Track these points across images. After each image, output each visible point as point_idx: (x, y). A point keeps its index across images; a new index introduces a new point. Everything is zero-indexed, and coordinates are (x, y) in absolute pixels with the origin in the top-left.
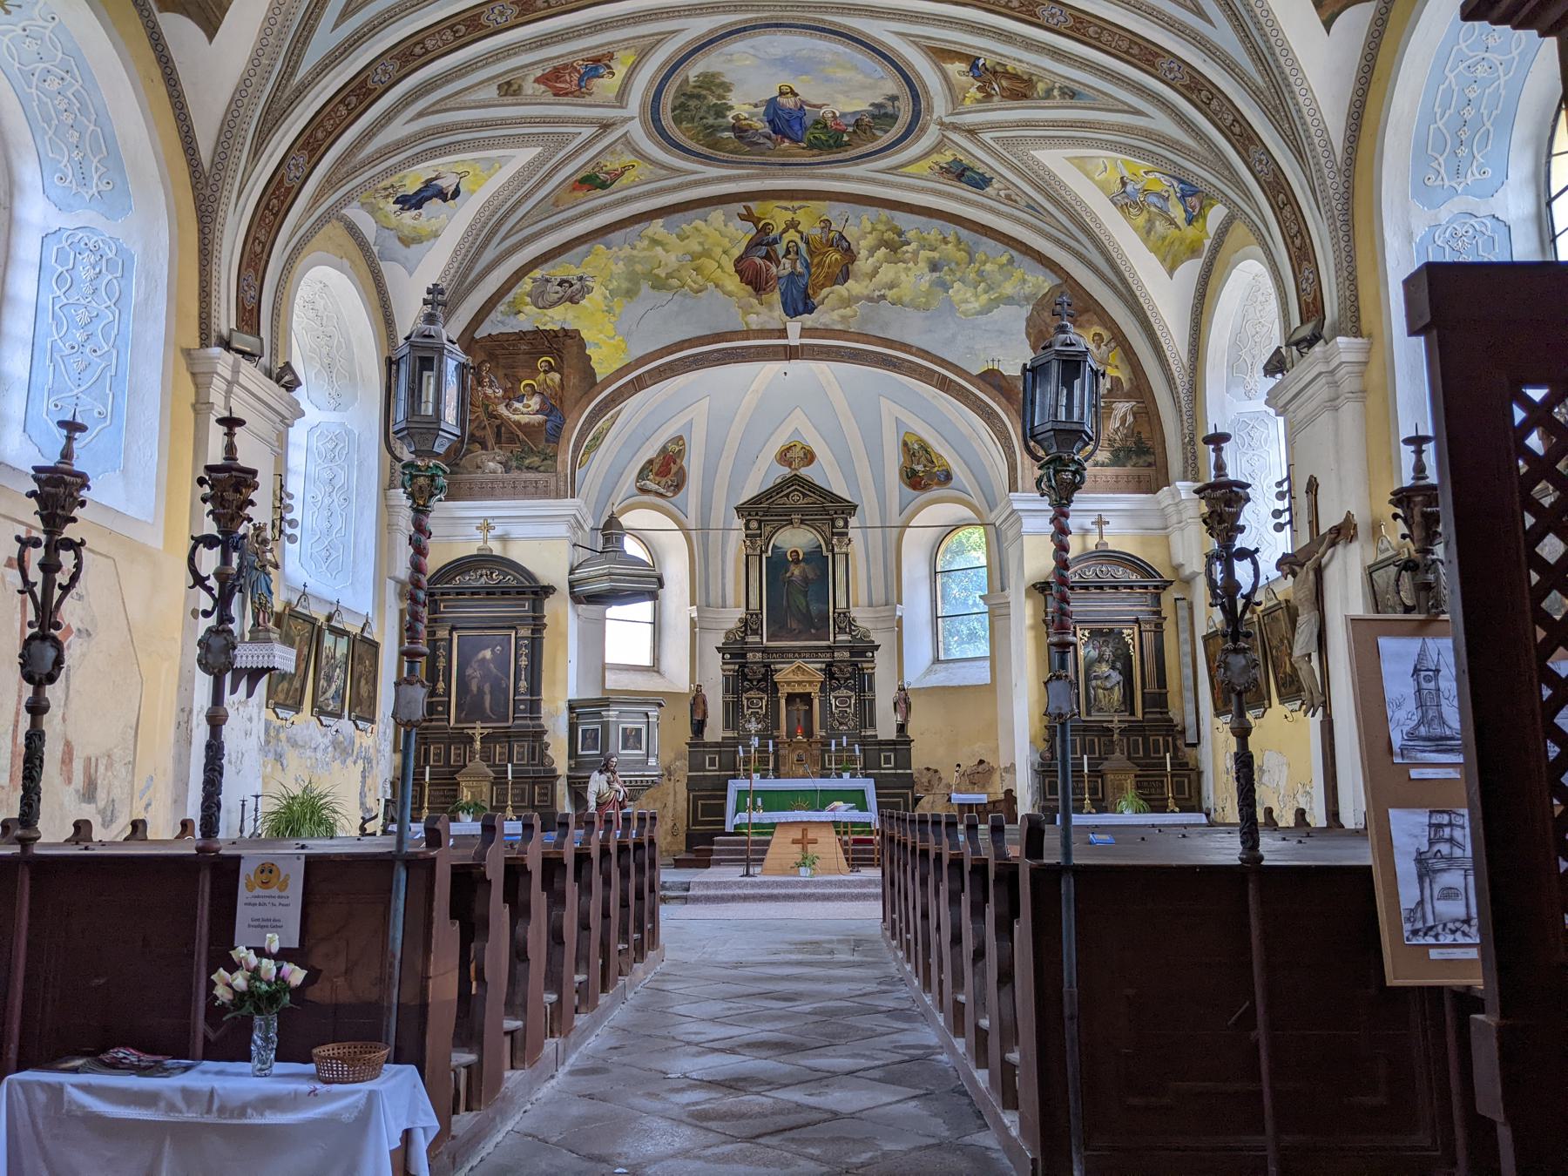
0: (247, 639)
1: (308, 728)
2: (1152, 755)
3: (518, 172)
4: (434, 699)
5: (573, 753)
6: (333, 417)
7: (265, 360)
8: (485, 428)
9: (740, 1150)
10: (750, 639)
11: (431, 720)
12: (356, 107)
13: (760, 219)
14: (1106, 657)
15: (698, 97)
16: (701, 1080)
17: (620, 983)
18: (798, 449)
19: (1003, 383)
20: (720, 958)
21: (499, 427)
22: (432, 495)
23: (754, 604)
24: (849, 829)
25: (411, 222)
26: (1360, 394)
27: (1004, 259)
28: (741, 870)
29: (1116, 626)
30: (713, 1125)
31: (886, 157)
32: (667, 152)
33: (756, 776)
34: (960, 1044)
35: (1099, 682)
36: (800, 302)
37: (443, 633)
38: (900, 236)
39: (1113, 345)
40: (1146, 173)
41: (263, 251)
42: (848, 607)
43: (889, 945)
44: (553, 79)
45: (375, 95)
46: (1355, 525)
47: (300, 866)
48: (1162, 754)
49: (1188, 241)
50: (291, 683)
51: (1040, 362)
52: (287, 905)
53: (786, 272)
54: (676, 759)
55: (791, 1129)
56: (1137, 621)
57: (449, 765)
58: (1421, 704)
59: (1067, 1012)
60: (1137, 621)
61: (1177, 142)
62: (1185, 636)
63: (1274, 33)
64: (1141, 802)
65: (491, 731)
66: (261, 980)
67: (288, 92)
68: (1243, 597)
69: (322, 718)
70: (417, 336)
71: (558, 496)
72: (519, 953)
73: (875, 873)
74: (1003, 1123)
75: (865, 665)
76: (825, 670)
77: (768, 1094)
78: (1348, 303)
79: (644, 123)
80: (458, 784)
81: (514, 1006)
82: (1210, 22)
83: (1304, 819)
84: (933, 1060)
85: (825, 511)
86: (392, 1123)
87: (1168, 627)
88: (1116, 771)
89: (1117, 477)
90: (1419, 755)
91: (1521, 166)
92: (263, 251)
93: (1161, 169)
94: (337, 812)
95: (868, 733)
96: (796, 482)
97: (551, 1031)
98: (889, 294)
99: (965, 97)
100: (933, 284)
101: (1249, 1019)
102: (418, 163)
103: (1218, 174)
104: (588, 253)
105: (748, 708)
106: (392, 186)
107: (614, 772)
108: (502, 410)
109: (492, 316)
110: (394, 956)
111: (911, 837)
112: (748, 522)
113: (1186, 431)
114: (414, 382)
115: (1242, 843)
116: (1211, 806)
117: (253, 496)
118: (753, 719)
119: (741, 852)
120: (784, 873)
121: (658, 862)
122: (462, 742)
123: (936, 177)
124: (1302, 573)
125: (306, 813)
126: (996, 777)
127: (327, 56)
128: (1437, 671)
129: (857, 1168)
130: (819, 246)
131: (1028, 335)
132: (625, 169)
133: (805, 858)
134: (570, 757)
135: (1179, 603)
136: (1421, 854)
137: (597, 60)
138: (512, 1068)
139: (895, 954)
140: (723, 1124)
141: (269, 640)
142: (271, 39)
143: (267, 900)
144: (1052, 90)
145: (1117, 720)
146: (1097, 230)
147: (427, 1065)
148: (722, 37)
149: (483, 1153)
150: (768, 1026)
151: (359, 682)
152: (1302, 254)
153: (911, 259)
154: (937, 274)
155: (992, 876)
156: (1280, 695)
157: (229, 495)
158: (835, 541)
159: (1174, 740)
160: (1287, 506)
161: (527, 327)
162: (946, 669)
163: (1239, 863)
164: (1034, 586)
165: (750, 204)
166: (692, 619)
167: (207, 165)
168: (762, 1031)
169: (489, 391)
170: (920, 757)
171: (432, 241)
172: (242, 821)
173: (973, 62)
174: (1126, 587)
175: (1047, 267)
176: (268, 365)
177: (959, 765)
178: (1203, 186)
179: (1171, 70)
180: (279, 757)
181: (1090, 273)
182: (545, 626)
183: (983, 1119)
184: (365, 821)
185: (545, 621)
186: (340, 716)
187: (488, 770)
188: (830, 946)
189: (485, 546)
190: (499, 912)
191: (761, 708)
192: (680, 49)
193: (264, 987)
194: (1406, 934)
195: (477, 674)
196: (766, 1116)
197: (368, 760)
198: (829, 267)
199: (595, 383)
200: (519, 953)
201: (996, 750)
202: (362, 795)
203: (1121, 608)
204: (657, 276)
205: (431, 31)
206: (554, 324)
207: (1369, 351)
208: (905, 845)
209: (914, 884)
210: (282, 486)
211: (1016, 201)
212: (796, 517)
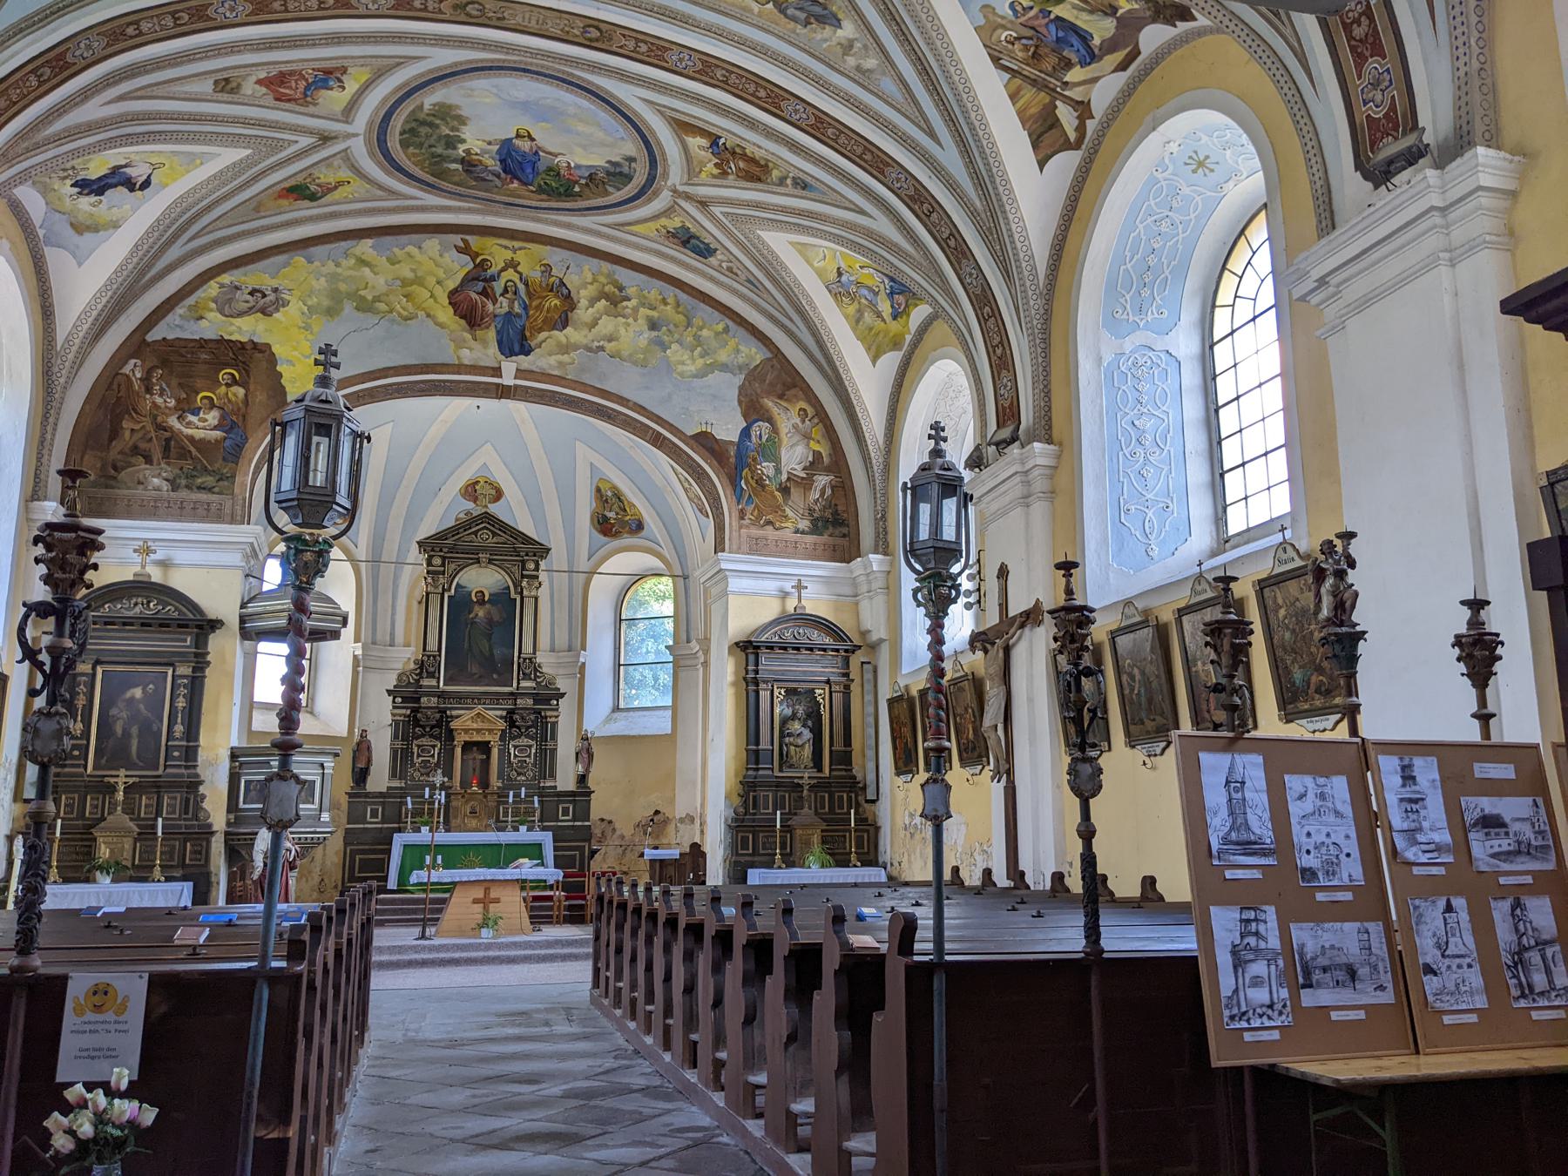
2: (761, 852)
5: (232, 806)
8: (151, 439)
10: (426, 682)
12: (49, 80)
13: (477, 255)
14: (799, 715)
15: (431, 125)
19: (716, 447)
23: (432, 645)
25: (88, 208)
27: (720, 327)
28: (417, 931)
32: (388, 173)
36: (516, 343)
38: (621, 291)
39: (816, 420)
40: (861, 267)
44: (278, 84)
51: (920, 482)
52: (125, 1031)
56: (828, 682)
58: (1231, 813)
59: (937, 1105)
60: (828, 682)
61: (896, 245)
62: (869, 697)
65: (137, 780)
71: (232, 521)
73: (583, 933)
75: (549, 713)
79: (368, 142)
80: (95, 840)
82: (939, 144)
83: (990, 879)
84: (718, 1143)
85: (516, 552)
88: (804, 827)
90: (1232, 857)
91: (1190, 313)
93: (874, 265)
95: (548, 784)
98: (609, 346)
99: (701, 171)
101: (1088, 1101)
102: (110, 148)
103: (927, 277)
105: (419, 756)
108: (173, 422)
109: (169, 318)
115: (1086, 937)
119: (415, 912)
120: (462, 934)
122: (99, 792)
123: (661, 240)
124: (993, 651)
127: (25, 19)
128: (1243, 783)
131: (740, 402)
132: (339, 184)
134: (229, 811)
135: (865, 666)
136: (1235, 946)
137: (328, 72)
143: (99, 1027)
144: (786, 178)
145: (806, 776)
152: (1002, 363)
153: (630, 315)
154: (656, 333)
156: (961, 759)
157: (72, 557)
158: (524, 584)
161: (210, 335)
164: (737, 644)
165: (468, 237)
166: (355, 657)
169: (159, 400)
170: (597, 809)
171: (111, 231)
173: (714, 140)
174: (820, 649)
175: (759, 340)
179: (898, 180)
181: (800, 352)
182: (208, 663)
189: (143, 572)
191: (433, 756)
192: (422, 75)
194: (1226, 1020)
198: (548, 311)
201: (672, 801)
203: (816, 670)
204: (363, 298)
207: (1059, 457)
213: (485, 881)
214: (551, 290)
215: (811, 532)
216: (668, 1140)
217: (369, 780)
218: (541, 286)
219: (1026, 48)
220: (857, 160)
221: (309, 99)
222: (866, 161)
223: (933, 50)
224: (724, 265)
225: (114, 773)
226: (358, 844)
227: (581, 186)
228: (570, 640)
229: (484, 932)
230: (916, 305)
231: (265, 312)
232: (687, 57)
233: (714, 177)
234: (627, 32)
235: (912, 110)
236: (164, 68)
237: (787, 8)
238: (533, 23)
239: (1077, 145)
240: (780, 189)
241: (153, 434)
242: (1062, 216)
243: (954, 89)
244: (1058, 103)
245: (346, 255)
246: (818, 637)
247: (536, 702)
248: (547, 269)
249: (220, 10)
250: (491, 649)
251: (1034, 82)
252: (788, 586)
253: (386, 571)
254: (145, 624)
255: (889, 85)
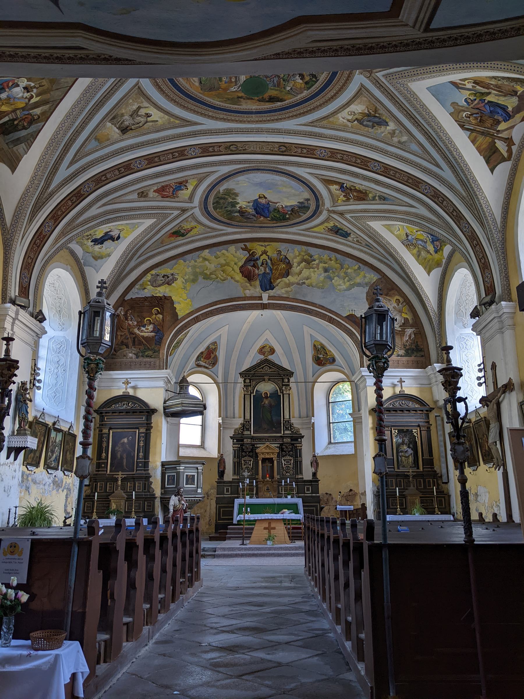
0: (15, 434)
1: (42, 475)
2: (391, 507)
3: (146, 229)
4: (100, 461)
5: (163, 486)
6: (61, 334)
7: (31, 309)
9: (234, 682)
11: (99, 471)
12: (75, 202)
13: (250, 250)
14: (406, 442)
15: (224, 199)
16: (217, 647)
17: (181, 598)
18: (267, 347)
20: (229, 585)
21: (134, 338)
22: (97, 372)
23: (248, 417)
24: (290, 522)
26: (512, 327)
27: (356, 267)
28: (240, 542)
29: (410, 428)
30: (221, 669)
31: (304, 224)
32: (211, 221)
33: (248, 497)
34: (339, 629)
35: (403, 454)
37: (105, 431)
39: (404, 304)
41: (32, 262)
42: (290, 418)
43: (308, 578)
45: (84, 196)
46: (513, 384)
47: (29, 544)
48: (432, 487)
49: (436, 260)
50: (35, 454)
51: (368, 314)
53: (262, 272)
54: (211, 489)
55: (258, 671)
56: (419, 426)
57: (106, 491)
59: (386, 615)
60: (419, 426)
61: (430, 219)
62: (440, 433)
63: (469, 174)
64: (423, 509)
65: (126, 476)
66: (7, 599)
67: (46, 195)
68: (461, 419)
69: (48, 470)
70: (93, 302)
72: (131, 585)
73: (301, 543)
74: (358, 668)
75: (298, 445)
76: (279, 447)
77: (248, 653)
78: (506, 287)
79: (201, 209)
80: (110, 501)
81: (129, 610)
82: (442, 169)
83: (497, 518)
84: (327, 636)
86: (66, 671)
87: (433, 428)
89: (408, 361)
92: (32, 262)
94: (53, 515)
95: (299, 477)
96: (266, 362)
97: (147, 623)
98: (307, 282)
100: (325, 278)
104: (176, 264)
105: (244, 465)
106: (91, 235)
107: (181, 496)
108: (136, 331)
110: (71, 587)
111: (317, 528)
112: (245, 379)
113: (438, 342)
114: (91, 322)
115: (465, 533)
116: (455, 511)
117: (16, 372)
118: (246, 470)
121: (200, 537)
123: (326, 233)
124: (491, 405)
125: (38, 515)
126: (358, 498)
127: (64, 180)
129: (289, 691)
130: (276, 261)
131: (367, 299)
133: (270, 536)
134: (162, 489)
137: (181, 183)
138: (127, 641)
139: (310, 583)
140: (227, 669)
141: (25, 434)
142: (39, 173)
143: (12, 561)
144: (375, 196)
145: (411, 471)
146: (396, 255)
147: (85, 641)
148: (234, 174)
149: (111, 684)
150: (249, 619)
151: (66, 453)
152: (485, 266)
153: (316, 267)
154: (327, 274)
155: (351, 549)
156: (483, 460)
157: (5, 372)
158: (284, 388)
159: (437, 481)
160: (483, 375)
161: (148, 295)
162: (334, 447)
163: (464, 543)
164: (372, 409)
166: (219, 423)
167: (8, 225)
168: (247, 622)
169: (130, 323)
170: (323, 488)
172: (9, 519)
173: (341, 185)
174: (413, 411)
176: (32, 311)
177: (340, 492)
178: (441, 237)
179: (426, 189)
180: (27, 489)
183: (349, 666)
184: (66, 518)
185: (152, 425)
186: (57, 469)
187: (124, 494)
188: (280, 579)
190: (122, 566)
191: (250, 465)
193: (9, 603)
195: (121, 449)
196: (246, 665)
197: (69, 490)
199: (178, 319)
200: (131, 585)
201: (357, 485)
202: (66, 506)
204: (206, 274)
205: (109, 170)
206: (160, 293)
208: (314, 531)
209: (318, 550)
210: (35, 364)
211: (361, 243)
212: (266, 378)
213: (268, 519)
214: (281, 261)
215: (406, 355)
216: (304, 633)
217: (225, 475)
218: (277, 260)
219: (476, 118)
220: (406, 183)
221: (175, 195)
222: (410, 183)
223: (432, 127)
224: (355, 239)
225: (117, 473)
226: (222, 504)
227: (289, 214)
228: (307, 413)
229: (268, 542)
230: (445, 245)
231: (169, 284)
232: (324, 151)
233: (344, 201)
234: (297, 146)
235: (426, 156)
236: (118, 191)
237: (363, 122)
238: (258, 148)
239: (509, 159)
240: (373, 202)
241: (129, 336)
242: (506, 193)
243: (444, 143)
244: (496, 141)
245: (199, 257)
246: (412, 405)
247: (292, 440)
248: (280, 252)
249: (135, 165)
250: (271, 418)
251: (482, 133)
252: (395, 381)
253: (230, 386)
254: (127, 412)
255: (414, 147)
